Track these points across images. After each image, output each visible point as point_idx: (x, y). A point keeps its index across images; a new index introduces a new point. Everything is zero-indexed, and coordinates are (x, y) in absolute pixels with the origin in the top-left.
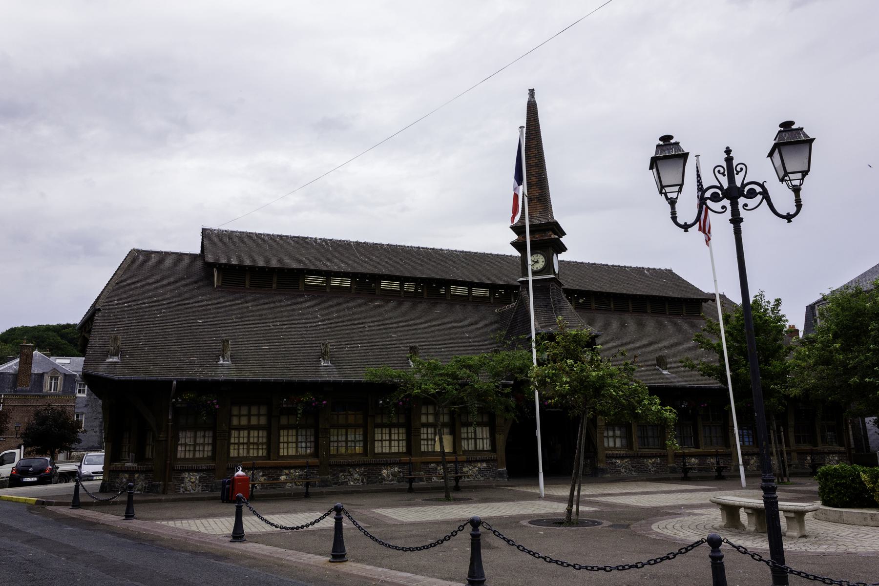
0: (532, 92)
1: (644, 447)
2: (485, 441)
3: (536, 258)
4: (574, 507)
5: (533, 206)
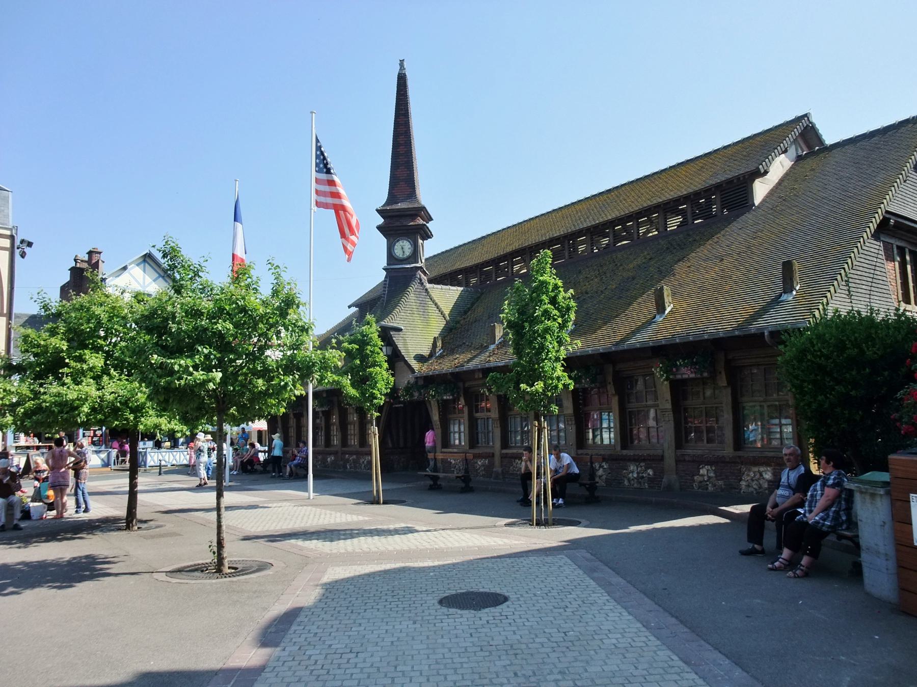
0: (402, 62)
2: (462, 434)
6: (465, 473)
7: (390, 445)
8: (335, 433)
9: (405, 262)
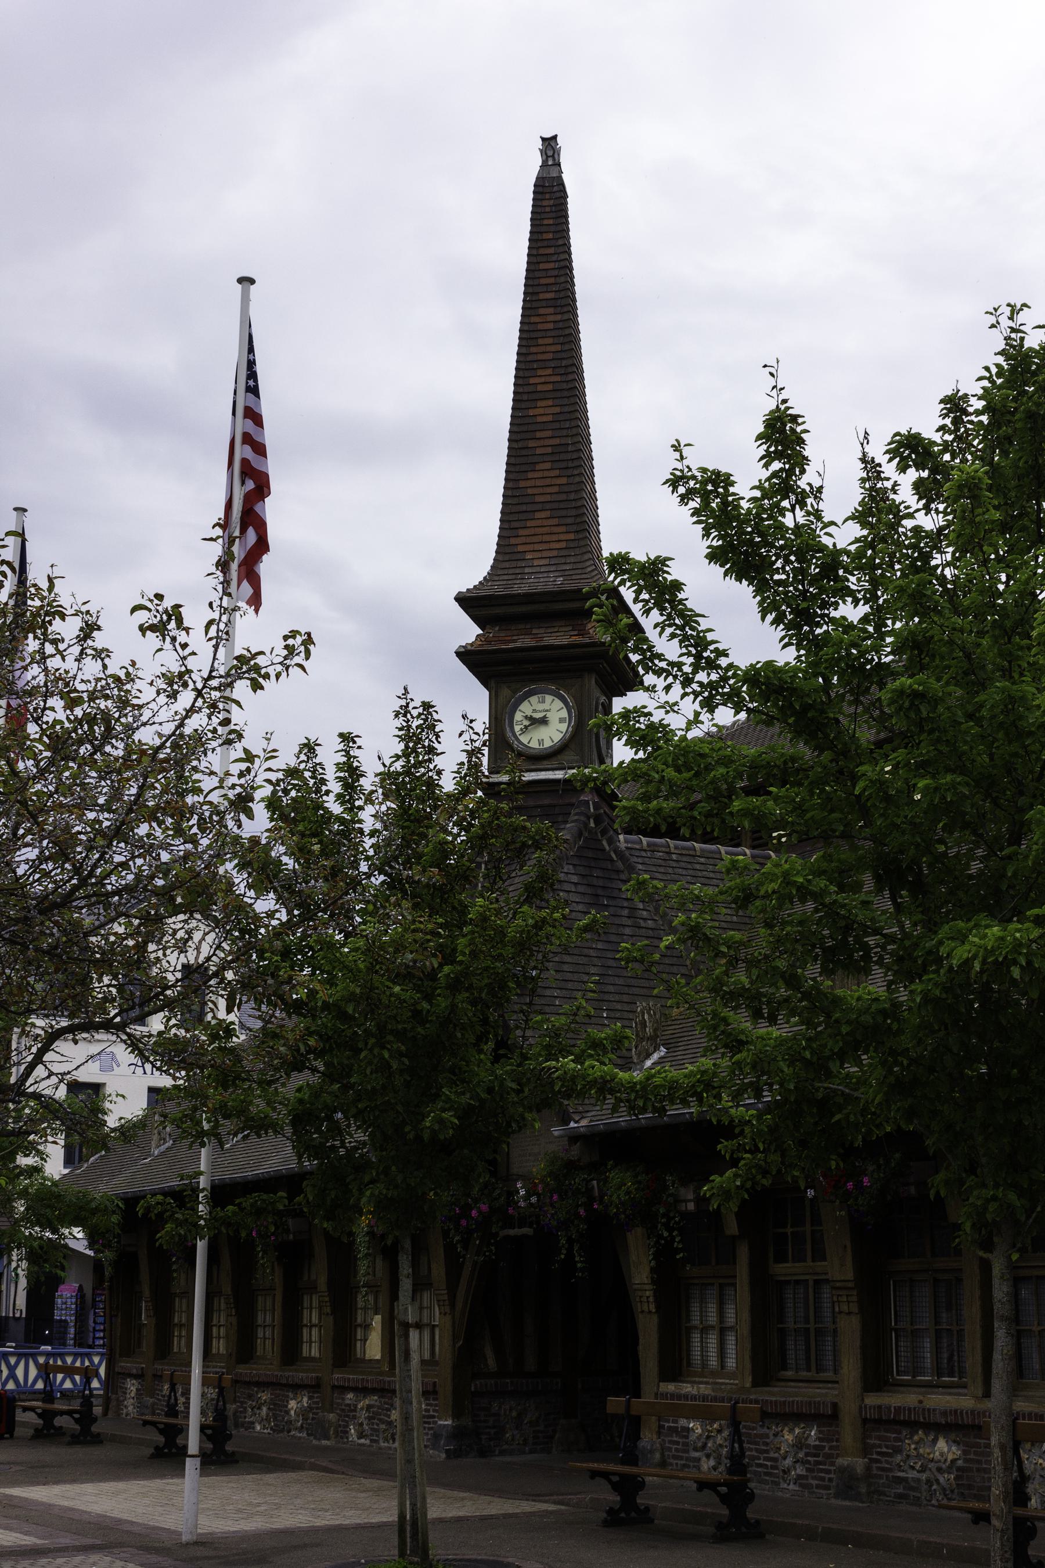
0: (550, 146)
1: (804, 1374)
2: (731, 1339)
3: (541, 707)
4: (83, 903)
5: (539, 483)
6: (730, 1471)
7: (492, 1363)
8: (315, 1320)
9: (545, 764)
